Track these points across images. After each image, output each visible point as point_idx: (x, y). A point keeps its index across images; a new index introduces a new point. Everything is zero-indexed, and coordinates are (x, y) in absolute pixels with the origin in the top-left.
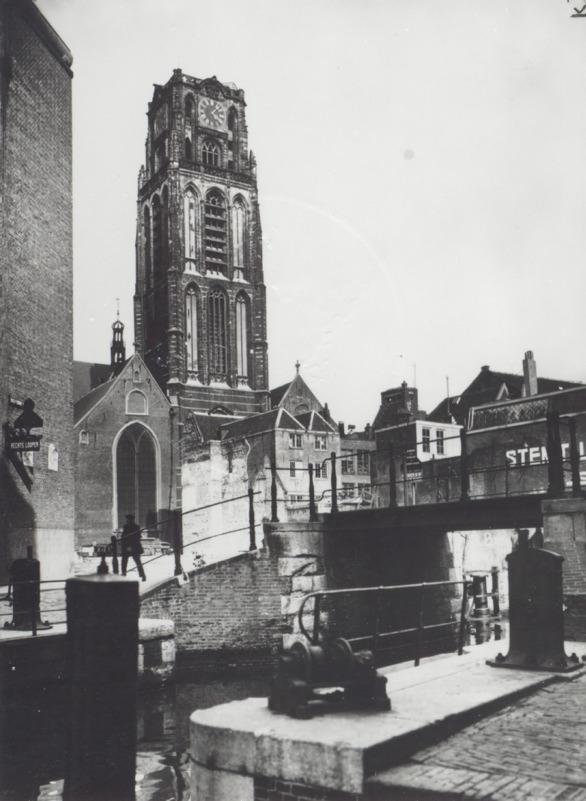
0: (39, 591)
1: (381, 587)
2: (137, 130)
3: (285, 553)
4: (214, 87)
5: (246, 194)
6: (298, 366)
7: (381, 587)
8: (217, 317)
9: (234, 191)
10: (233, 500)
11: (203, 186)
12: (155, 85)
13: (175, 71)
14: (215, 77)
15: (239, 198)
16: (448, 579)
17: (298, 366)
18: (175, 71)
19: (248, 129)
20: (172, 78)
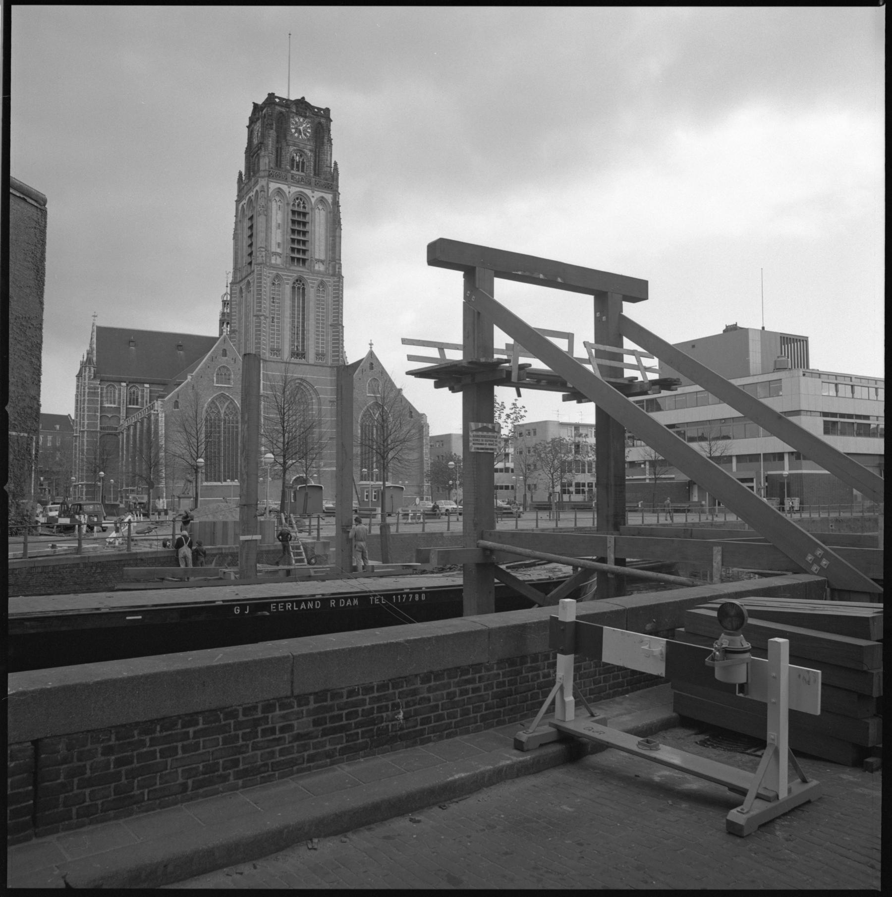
0: (884, 608)
1: (19, 806)
2: (556, 709)
3: (83, 551)
4: (303, 106)
5: (329, 197)
6: (371, 344)
7: (19, 806)
8: (298, 318)
9: (318, 194)
10: (765, 771)
11: (291, 190)
12: (254, 103)
13: (269, 94)
14: (303, 98)
15: (322, 200)
16: (667, 641)
17: (371, 344)
18: (269, 94)
19: (333, 141)
20: (267, 100)
